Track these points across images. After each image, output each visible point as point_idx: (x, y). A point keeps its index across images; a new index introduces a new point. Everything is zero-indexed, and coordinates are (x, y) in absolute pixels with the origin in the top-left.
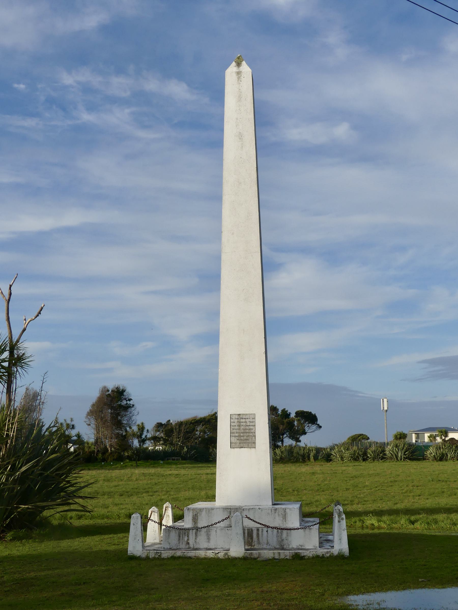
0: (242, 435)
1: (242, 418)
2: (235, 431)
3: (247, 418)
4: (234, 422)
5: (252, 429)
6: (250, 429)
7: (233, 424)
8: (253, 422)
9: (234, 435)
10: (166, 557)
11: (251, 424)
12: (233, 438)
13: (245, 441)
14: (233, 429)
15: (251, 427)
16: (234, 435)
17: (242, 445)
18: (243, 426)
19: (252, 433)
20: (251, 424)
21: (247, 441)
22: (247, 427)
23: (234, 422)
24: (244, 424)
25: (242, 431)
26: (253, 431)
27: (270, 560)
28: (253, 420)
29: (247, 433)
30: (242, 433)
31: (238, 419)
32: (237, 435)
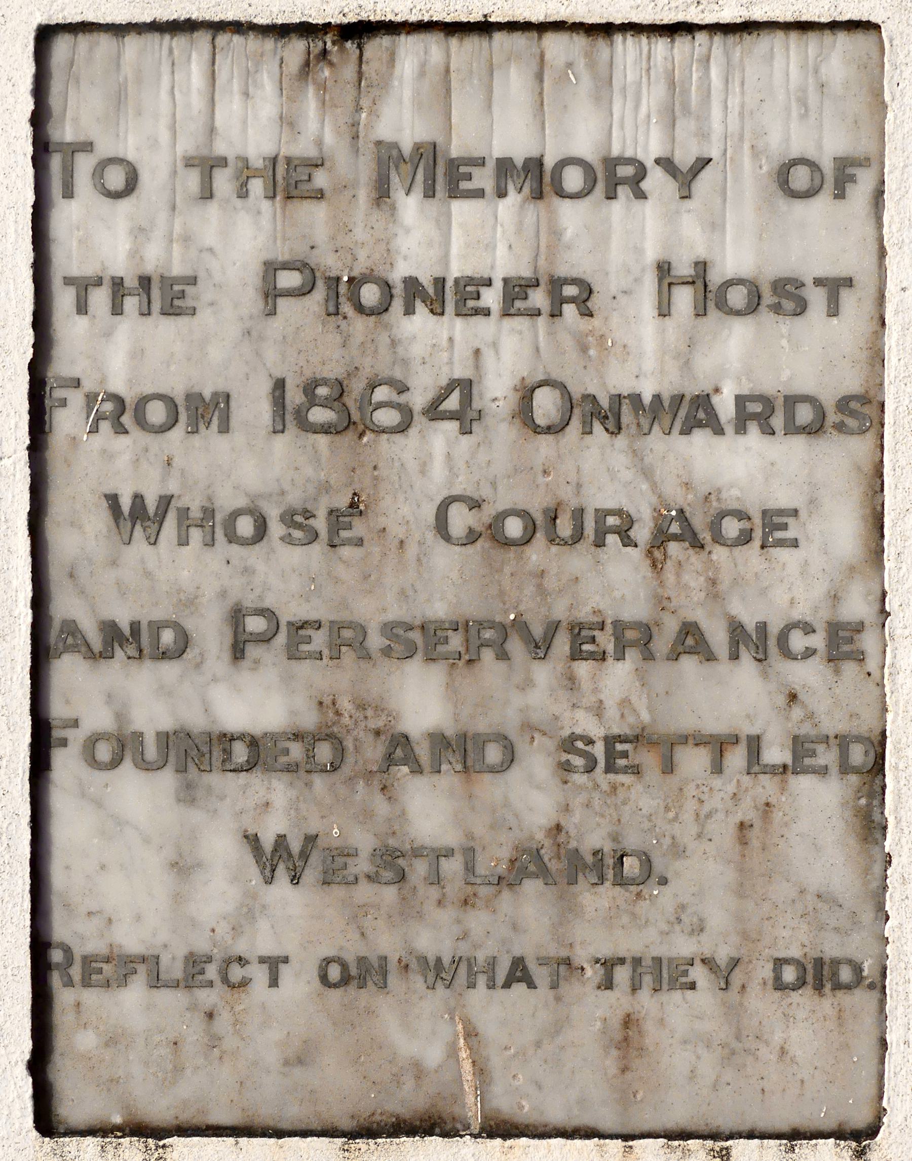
0: (421, 700)
1: (443, 173)
2: (182, 575)
3: (616, 177)
4: (164, 295)
5: (772, 528)
6: (681, 531)
7: (108, 352)
8: (784, 296)
9: (150, 699)
10: (293, 35)
11: (736, 356)
12: (141, 796)
13: (528, 919)
14: (134, 517)
15: (739, 466)
16: (150, 699)
17: (417, 1034)
18: (458, 403)
19: (755, 642)
20: (736, 356)
21: (600, 923)
22: (603, 473)
23: (164, 295)
24: (505, 352)
25: (446, 583)
26: (787, 586)
27: (405, 287)
28: (817, 239)
29: (584, 640)
30: (422, 640)
31: (290, 181)
32: (256, 701)
